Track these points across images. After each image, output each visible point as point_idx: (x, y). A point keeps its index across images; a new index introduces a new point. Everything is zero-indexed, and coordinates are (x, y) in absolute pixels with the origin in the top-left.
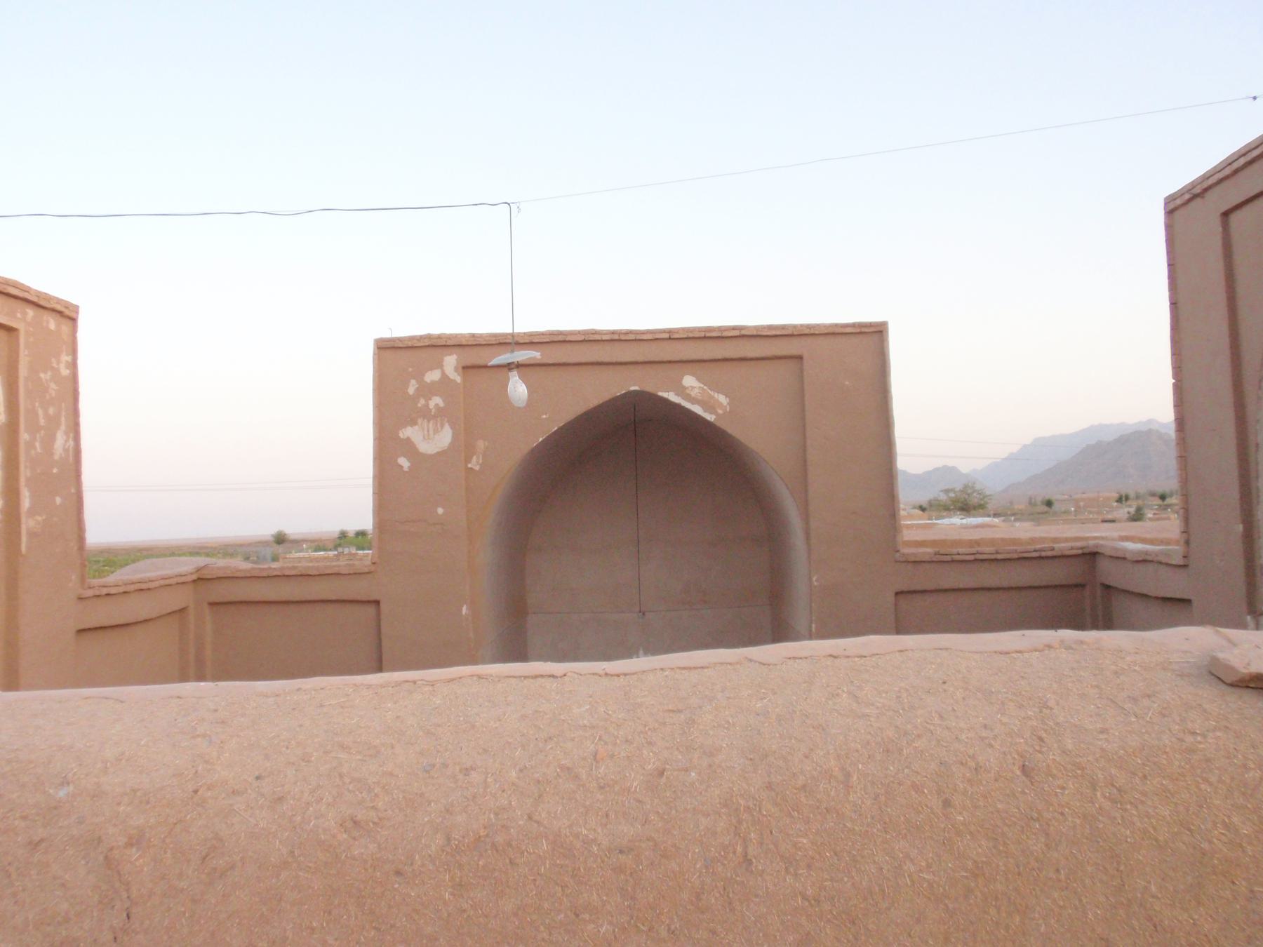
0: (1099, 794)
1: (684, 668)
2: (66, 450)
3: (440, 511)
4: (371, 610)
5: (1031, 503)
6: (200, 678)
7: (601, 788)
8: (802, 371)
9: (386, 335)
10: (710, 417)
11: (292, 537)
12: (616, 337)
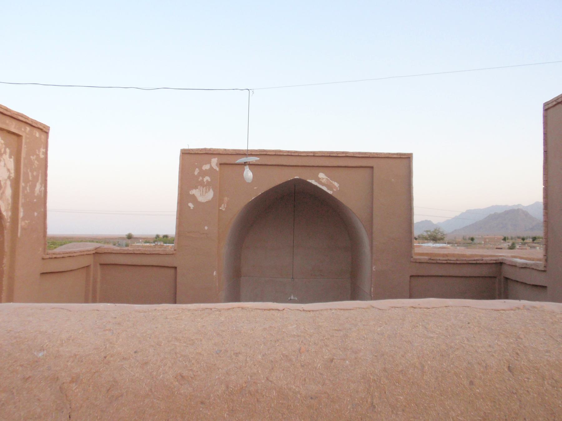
0: (546, 382)
1: (341, 309)
2: (40, 192)
3: (206, 228)
4: (172, 271)
5: (464, 239)
6: (94, 301)
7: (302, 366)
8: (373, 174)
9: (186, 147)
10: (330, 192)
11: (135, 236)
12: (290, 154)
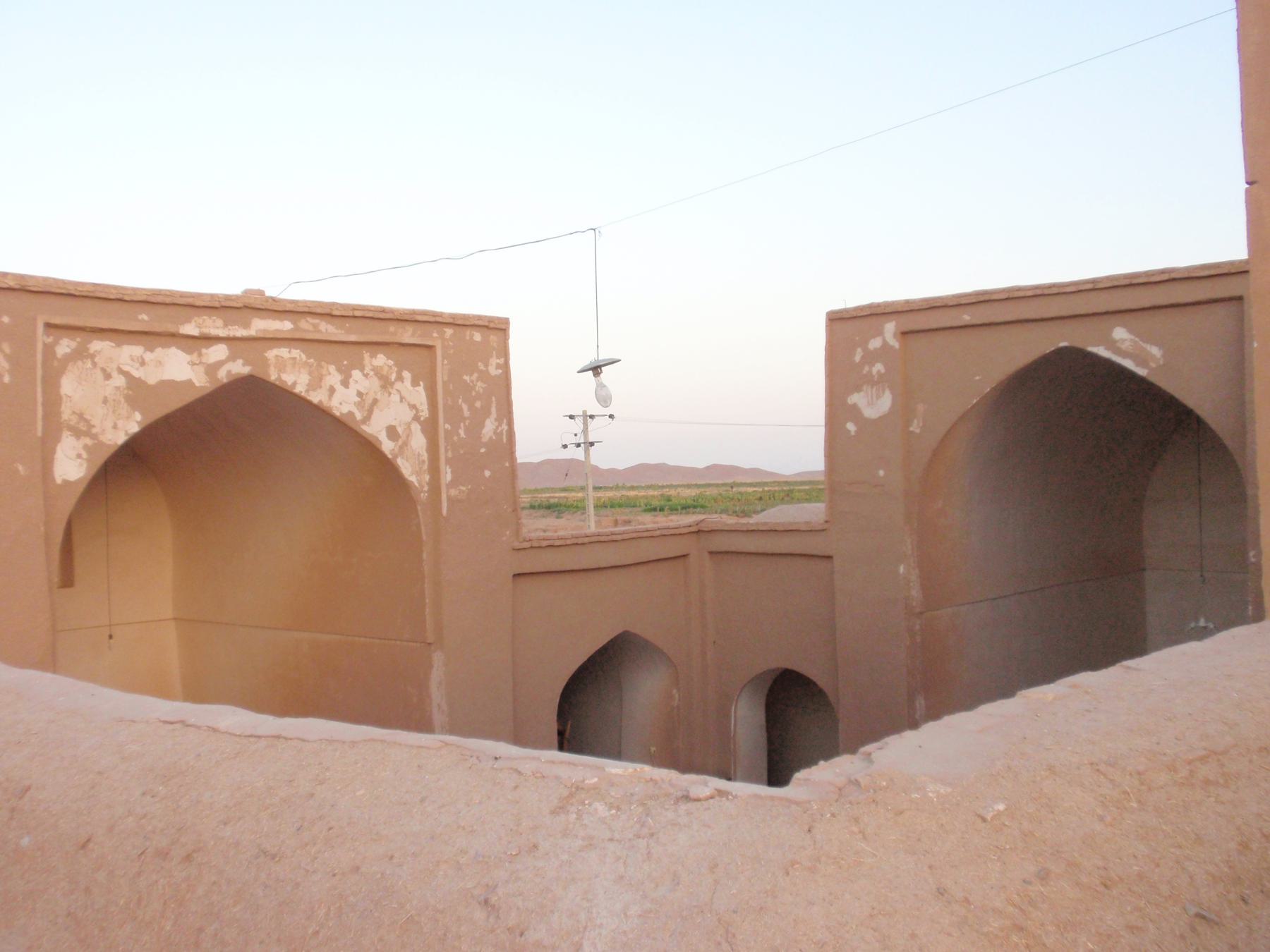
10: (1142, 372)
12: (1039, 292)
